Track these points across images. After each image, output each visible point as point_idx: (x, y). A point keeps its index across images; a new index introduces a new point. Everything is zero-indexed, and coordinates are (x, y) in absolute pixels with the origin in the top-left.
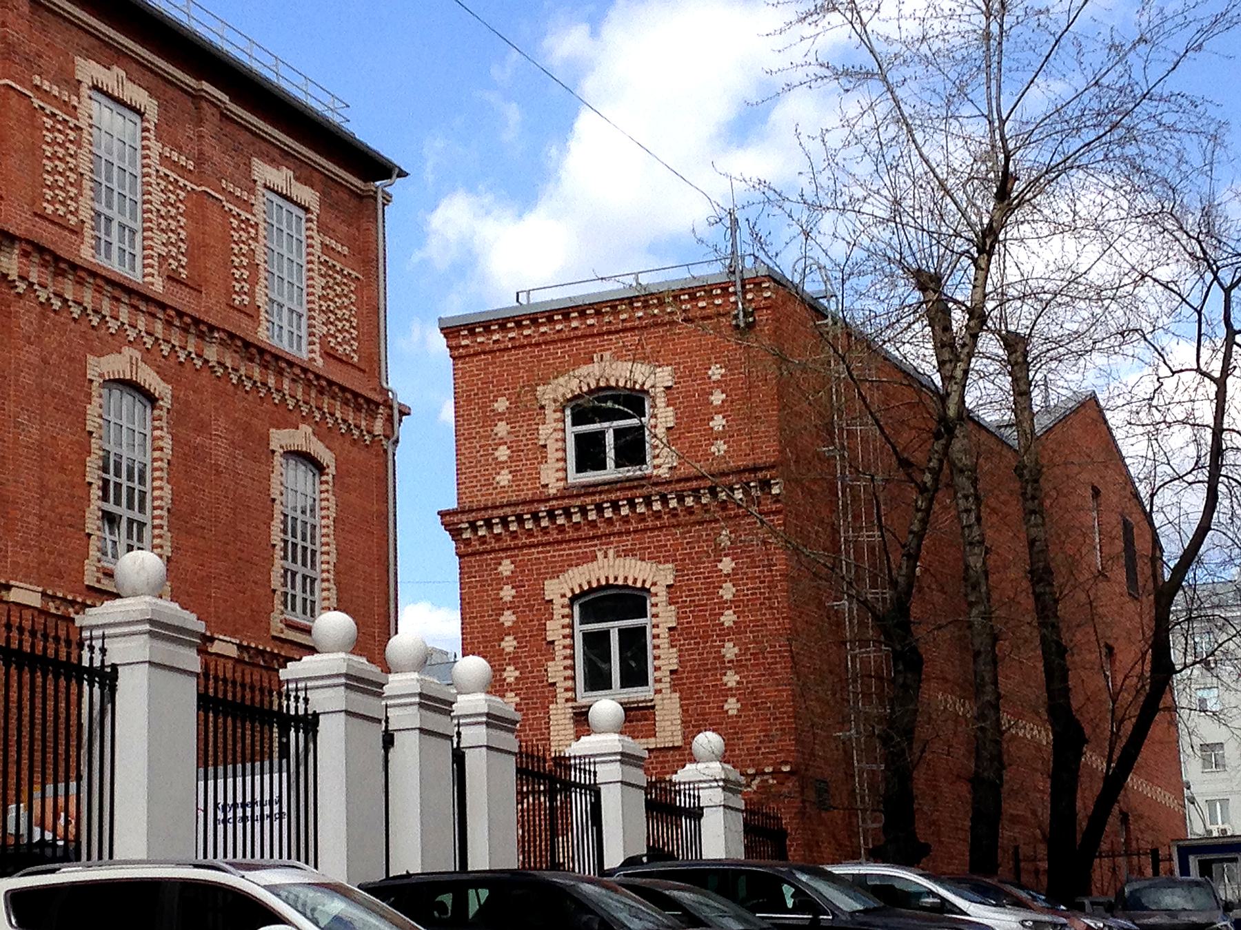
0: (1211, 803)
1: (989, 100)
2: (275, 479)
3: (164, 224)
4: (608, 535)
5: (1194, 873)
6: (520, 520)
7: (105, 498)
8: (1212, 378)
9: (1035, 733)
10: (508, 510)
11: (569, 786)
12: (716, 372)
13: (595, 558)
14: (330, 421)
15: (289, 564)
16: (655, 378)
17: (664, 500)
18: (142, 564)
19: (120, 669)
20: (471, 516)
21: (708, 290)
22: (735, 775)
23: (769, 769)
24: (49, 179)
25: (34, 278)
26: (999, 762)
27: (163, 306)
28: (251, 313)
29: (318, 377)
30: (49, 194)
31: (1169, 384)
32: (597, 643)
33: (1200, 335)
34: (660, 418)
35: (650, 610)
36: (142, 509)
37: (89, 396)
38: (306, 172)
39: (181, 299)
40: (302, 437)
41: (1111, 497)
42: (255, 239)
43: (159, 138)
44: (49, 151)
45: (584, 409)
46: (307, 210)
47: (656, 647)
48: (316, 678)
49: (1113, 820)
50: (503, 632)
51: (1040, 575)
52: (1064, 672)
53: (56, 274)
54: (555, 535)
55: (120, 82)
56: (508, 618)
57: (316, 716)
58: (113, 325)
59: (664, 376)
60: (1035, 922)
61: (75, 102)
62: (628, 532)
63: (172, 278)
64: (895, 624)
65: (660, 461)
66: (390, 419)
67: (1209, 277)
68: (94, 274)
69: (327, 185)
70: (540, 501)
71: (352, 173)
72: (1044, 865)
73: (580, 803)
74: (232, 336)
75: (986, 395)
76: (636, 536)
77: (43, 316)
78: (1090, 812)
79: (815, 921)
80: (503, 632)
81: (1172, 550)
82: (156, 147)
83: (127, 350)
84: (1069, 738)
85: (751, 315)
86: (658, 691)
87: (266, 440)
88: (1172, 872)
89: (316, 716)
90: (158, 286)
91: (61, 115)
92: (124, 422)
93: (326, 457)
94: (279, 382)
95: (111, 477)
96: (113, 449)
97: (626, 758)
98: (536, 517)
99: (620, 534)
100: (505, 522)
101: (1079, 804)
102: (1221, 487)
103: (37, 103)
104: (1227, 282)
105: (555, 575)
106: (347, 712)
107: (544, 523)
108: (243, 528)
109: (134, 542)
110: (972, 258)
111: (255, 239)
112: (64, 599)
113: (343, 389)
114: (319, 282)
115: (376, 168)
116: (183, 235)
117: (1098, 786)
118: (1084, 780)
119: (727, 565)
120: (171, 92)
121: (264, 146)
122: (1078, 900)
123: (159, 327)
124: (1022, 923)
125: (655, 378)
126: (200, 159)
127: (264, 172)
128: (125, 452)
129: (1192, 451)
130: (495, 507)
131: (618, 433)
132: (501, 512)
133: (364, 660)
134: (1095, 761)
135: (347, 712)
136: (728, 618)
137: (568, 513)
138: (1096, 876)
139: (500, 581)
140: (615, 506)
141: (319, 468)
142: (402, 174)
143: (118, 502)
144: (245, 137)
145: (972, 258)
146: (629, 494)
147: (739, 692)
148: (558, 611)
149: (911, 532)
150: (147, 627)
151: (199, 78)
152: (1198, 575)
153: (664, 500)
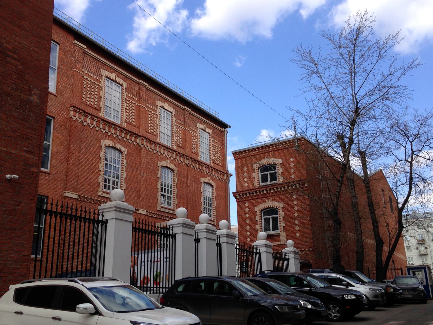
0: (409, 258)
1: (352, 90)
2: (202, 188)
3: (176, 135)
4: (269, 197)
5: (412, 275)
6: (249, 193)
7: (162, 191)
8: (409, 162)
9: (370, 242)
10: (247, 192)
11: (254, 253)
12: (292, 159)
13: (266, 202)
14: (214, 177)
15: (205, 206)
16: (278, 161)
17: (281, 188)
18: (118, 192)
19: (108, 220)
20: (239, 193)
21: (289, 141)
22: (298, 251)
23: (307, 249)
24: (150, 125)
25: (145, 144)
26: (362, 247)
27: (175, 151)
28: (197, 154)
29: (211, 167)
30: (150, 128)
31: (399, 164)
32: (267, 221)
33: (405, 152)
34: (280, 170)
35: (278, 213)
36: (211, 207)
37: (158, 170)
38: (209, 126)
39: (181, 151)
40: (208, 180)
41: (387, 192)
42: (197, 139)
43: (175, 118)
44: (150, 119)
45: (264, 168)
46: (209, 134)
47: (280, 221)
48: (201, 230)
49: (391, 262)
50: (246, 218)
51: (371, 205)
52: (378, 227)
53: (150, 144)
54: (257, 197)
55: (166, 106)
56: (247, 215)
57: (175, 234)
58: (164, 155)
59: (280, 161)
60: (373, 289)
61: (156, 109)
62: (273, 196)
63: (178, 146)
64: (335, 214)
65: (280, 179)
66: (228, 176)
67: (407, 140)
68: (159, 144)
69: (214, 129)
70: (254, 189)
71: (220, 126)
72: (375, 272)
73: (256, 257)
74: (191, 158)
75: (355, 164)
76: (275, 196)
77: (147, 153)
78: (385, 260)
79: (310, 290)
80: (246, 218)
81: (401, 200)
82: (174, 119)
83: (167, 160)
84: (380, 243)
85: (300, 147)
86: (281, 231)
87: (200, 180)
88: (406, 274)
89: (175, 234)
90: (175, 147)
91: (153, 112)
92: (166, 176)
93: (214, 184)
94: (202, 168)
95: (163, 187)
96: (164, 181)
97: (267, 246)
98: (253, 193)
99: (271, 196)
100: (246, 194)
101: (383, 258)
102: (413, 186)
103: (147, 109)
104: (411, 141)
105: (257, 206)
106: (183, 233)
107: (255, 194)
108: (194, 198)
109: (115, 186)
110: (349, 127)
111: (197, 139)
112: (152, 213)
113: (217, 170)
114: (212, 148)
115: (225, 126)
116: (181, 137)
117: (387, 254)
118: (384, 253)
119: (295, 202)
120: (178, 108)
121: (200, 121)
122: (384, 280)
123: (174, 156)
124: (370, 289)
125: (278, 161)
126: (185, 122)
127: (199, 125)
128: (167, 182)
129: (405, 179)
130: (244, 191)
131: (270, 174)
132: (245, 192)
133: (189, 220)
134: (386, 249)
135: (183, 233)
136: (296, 214)
137: (260, 192)
138: (388, 274)
139: (246, 207)
140: (270, 190)
141: (212, 186)
142: (230, 127)
143: (165, 192)
144: (195, 118)
145: (349, 127)
146: (273, 187)
147: (299, 231)
148: (258, 213)
149: (337, 192)
150: (115, 209)
151: (184, 106)
152: (408, 206)
153: (281, 188)
